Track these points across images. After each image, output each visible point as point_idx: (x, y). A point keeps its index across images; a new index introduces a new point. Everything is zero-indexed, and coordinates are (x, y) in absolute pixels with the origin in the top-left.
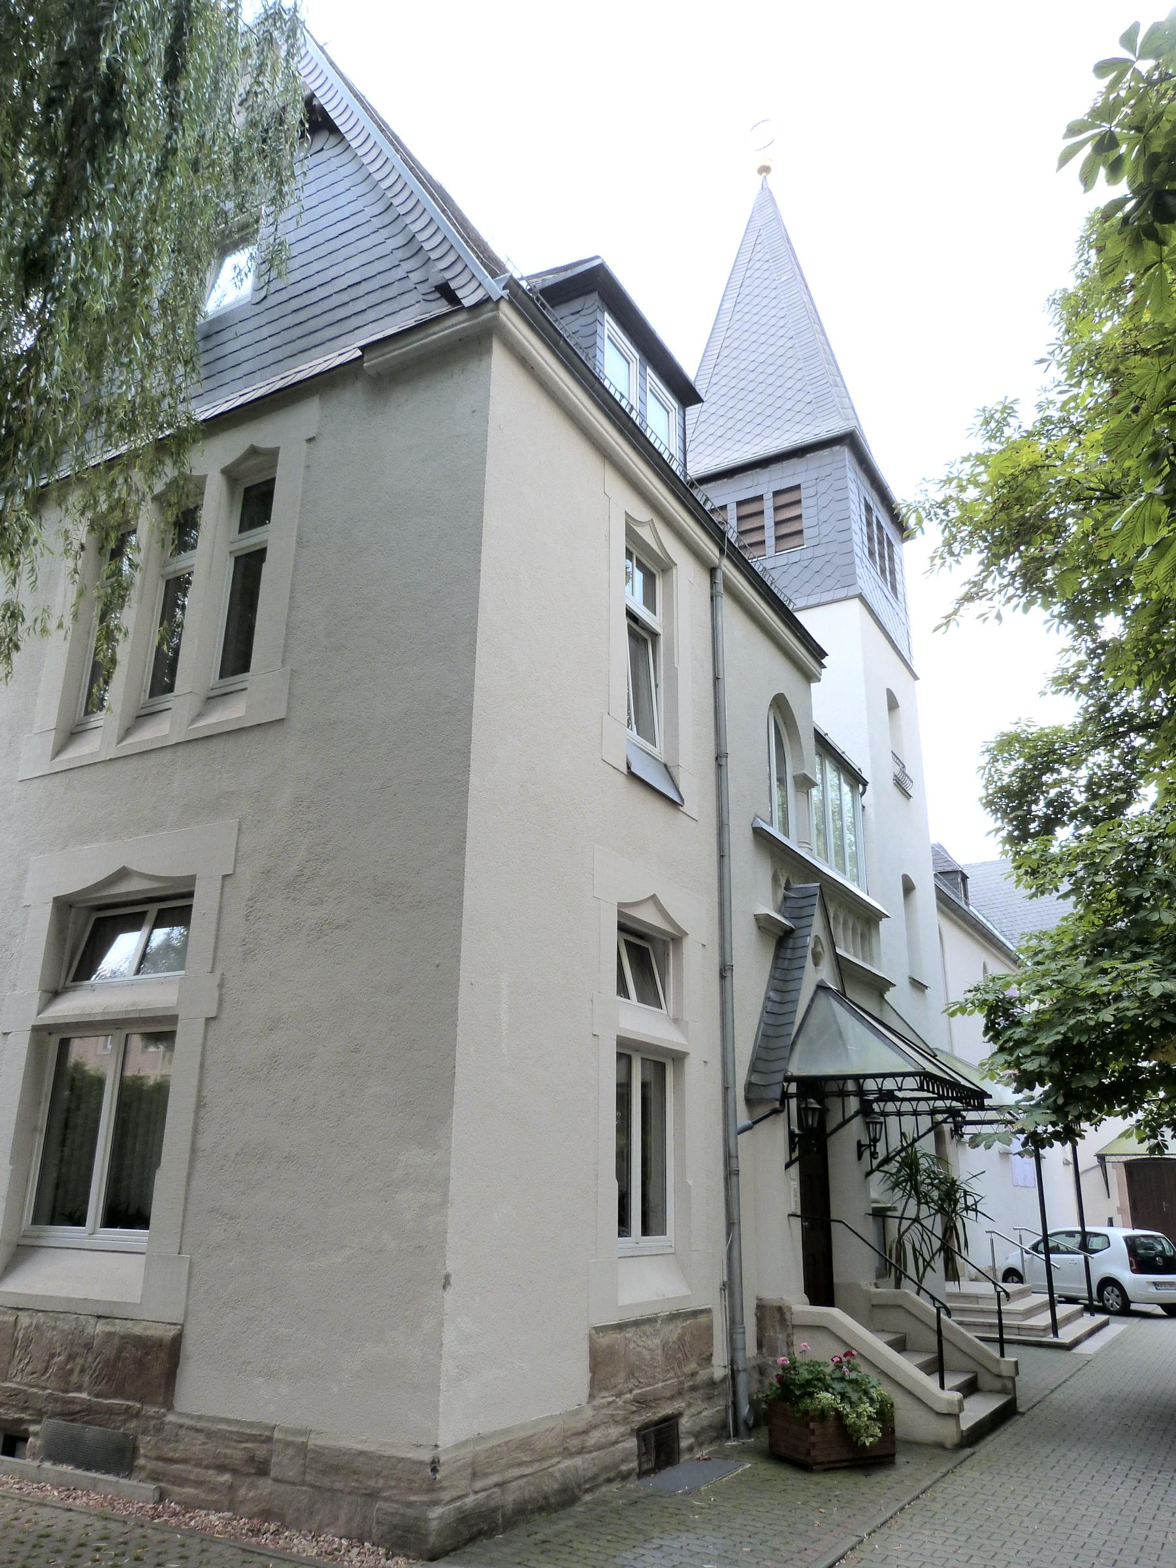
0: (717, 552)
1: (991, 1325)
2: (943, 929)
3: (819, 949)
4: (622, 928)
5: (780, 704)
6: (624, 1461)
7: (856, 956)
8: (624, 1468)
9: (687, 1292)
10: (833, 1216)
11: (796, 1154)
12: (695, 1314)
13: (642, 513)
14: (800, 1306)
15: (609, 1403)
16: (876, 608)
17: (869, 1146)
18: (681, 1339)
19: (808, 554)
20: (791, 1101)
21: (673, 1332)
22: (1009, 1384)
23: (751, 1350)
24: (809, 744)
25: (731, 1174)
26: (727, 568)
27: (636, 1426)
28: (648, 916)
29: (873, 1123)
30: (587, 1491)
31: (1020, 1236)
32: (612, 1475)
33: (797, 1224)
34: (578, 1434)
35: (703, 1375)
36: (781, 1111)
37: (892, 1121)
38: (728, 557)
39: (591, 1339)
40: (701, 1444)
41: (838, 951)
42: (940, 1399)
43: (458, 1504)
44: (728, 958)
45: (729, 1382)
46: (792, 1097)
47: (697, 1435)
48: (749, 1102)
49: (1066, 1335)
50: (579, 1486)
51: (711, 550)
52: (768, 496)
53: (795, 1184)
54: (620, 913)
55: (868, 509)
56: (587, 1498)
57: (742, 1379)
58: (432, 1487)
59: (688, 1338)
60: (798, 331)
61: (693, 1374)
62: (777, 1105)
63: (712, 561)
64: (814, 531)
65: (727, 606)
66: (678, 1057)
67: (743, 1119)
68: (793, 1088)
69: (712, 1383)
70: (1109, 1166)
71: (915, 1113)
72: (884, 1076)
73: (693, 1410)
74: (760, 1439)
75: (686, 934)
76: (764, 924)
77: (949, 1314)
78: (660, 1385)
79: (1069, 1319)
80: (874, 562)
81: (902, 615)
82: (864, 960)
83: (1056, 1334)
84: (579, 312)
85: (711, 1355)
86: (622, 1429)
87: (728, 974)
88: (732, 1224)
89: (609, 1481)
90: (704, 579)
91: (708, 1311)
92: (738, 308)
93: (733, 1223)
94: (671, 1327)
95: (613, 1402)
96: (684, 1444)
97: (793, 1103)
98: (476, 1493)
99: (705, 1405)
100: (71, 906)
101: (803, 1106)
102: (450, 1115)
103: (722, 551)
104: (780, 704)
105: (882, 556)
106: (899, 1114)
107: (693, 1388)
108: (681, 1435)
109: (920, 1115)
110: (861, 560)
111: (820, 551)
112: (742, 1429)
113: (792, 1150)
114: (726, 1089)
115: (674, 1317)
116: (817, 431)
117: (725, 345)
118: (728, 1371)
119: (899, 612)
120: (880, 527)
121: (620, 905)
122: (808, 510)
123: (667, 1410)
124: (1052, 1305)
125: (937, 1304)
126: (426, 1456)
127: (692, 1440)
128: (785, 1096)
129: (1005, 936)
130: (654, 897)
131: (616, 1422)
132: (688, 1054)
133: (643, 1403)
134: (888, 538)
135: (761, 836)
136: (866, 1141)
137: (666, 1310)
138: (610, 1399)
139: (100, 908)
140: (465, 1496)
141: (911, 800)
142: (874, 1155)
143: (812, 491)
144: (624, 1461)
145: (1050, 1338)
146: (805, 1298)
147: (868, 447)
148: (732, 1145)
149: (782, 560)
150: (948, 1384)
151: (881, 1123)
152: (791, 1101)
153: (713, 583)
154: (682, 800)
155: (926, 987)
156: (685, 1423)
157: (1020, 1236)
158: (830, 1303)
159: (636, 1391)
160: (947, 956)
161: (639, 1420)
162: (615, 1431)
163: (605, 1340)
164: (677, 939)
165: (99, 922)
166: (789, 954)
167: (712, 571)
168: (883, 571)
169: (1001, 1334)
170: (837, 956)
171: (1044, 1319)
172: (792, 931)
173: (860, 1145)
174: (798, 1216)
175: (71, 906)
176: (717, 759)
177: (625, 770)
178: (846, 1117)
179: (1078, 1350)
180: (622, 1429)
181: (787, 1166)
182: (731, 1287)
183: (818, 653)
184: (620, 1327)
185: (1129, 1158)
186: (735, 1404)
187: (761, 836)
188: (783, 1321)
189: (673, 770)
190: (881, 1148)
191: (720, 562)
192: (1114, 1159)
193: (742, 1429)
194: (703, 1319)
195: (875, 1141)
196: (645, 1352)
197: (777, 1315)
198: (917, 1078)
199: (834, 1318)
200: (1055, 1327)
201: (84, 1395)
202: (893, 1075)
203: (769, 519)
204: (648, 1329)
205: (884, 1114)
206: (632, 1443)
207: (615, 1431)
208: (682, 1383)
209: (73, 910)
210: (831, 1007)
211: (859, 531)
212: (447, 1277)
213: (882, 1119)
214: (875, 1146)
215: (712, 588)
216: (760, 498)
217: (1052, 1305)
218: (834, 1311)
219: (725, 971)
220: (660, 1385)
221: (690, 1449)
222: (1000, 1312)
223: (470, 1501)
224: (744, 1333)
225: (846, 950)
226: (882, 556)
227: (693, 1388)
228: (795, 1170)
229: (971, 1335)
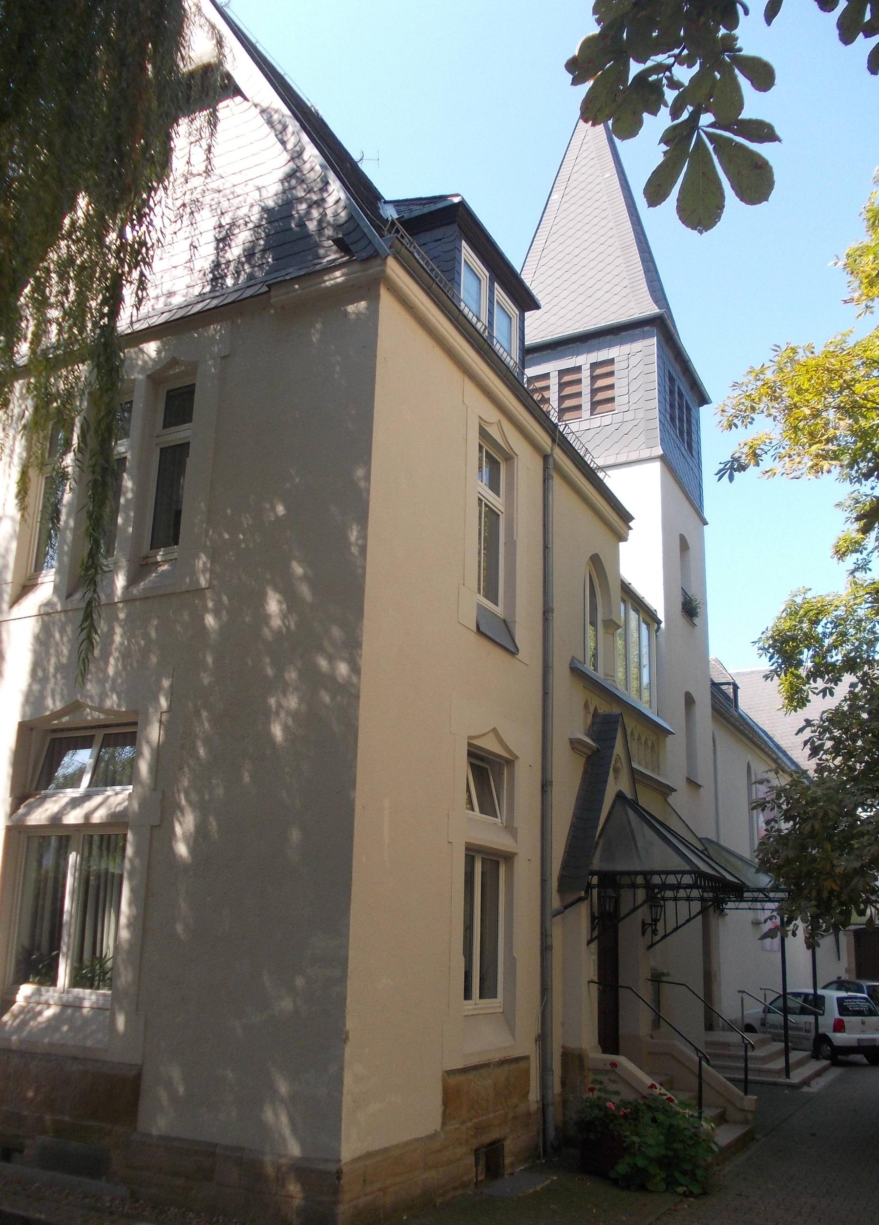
0: (549, 441)
1: (738, 1068)
2: (717, 736)
3: (619, 765)
4: (470, 754)
5: (595, 560)
7: (647, 768)
8: (466, 1179)
10: (620, 984)
11: (595, 934)
12: (517, 1060)
14: (595, 1054)
15: (456, 1129)
17: (651, 925)
19: (619, 418)
20: (593, 890)
23: (557, 1088)
24: (616, 592)
26: (559, 455)
28: (490, 745)
29: (654, 906)
31: (765, 995)
33: (595, 988)
36: (587, 899)
37: (670, 905)
38: (559, 445)
39: (444, 1080)
41: (635, 765)
43: (355, 1203)
46: (594, 888)
48: (561, 890)
49: (796, 1077)
51: (544, 440)
53: (595, 957)
54: (469, 744)
55: (671, 379)
57: (551, 1110)
58: (336, 1191)
60: (618, 223)
61: (516, 1106)
62: (583, 894)
64: (625, 399)
65: (557, 483)
66: (509, 857)
67: (556, 902)
68: (595, 880)
69: (528, 1114)
71: (689, 899)
72: (668, 873)
75: (517, 757)
77: (708, 1062)
78: (492, 1115)
79: (801, 1063)
80: (675, 426)
82: (653, 770)
83: (788, 1076)
85: (528, 1092)
91: (526, 1058)
93: (546, 988)
95: (459, 1128)
97: (595, 892)
98: (365, 1195)
100: (32, 729)
101: (602, 894)
103: (554, 441)
104: (595, 560)
105: (681, 420)
106: (676, 899)
108: (506, 1154)
109: (692, 900)
111: (629, 416)
113: (593, 929)
115: (503, 1062)
116: (631, 312)
117: (555, 223)
120: (681, 395)
121: (470, 738)
123: (494, 1135)
124: (786, 1052)
125: (700, 1055)
126: (333, 1168)
128: (589, 887)
130: (494, 730)
132: (516, 854)
134: (687, 403)
135: (576, 672)
136: (649, 921)
137: (497, 1057)
138: (457, 1126)
139: (55, 731)
140: (359, 1197)
141: (696, 628)
142: (655, 932)
143: (624, 365)
147: (675, 326)
149: (597, 422)
151: (662, 907)
152: (593, 890)
154: (518, 650)
155: (700, 786)
156: (508, 1144)
157: (765, 995)
158: (616, 1052)
159: (475, 1121)
160: (718, 753)
161: (475, 1143)
163: (453, 1081)
164: (510, 763)
165: (53, 741)
167: (546, 458)
168: (681, 433)
169: (746, 1075)
171: (780, 1064)
173: (644, 924)
174: (596, 983)
175: (32, 729)
176: (544, 614)
177: (474, 628)
178: (636, 906)
181: (589, 942)
182: (543, 1039)
183: (626, 518)
184: (464, 1070)
186: (544, 1130)
187: (576, 672)
188: (582, 1066)
189: (510, 625)
190: (660, 926)
191: (552, 449)
194: (522, 1064)
195: (655, 921)
198: (700, 890)
200: (787, 1070)
201: (67, 1118)
202: (674, 873)
204: (483, 1071)
205: (664, 899)
206: (471, 1160)
209: (34, 732)
210: (627, 814)
213: (662, 902)
214: (656, 925)
215: (544, 471)
217: (786, 1052)
218: (621, 1059)
219: (546, 786)
220: (492, 1115)
222: (746, 1059)
223: (362, 1201)
224: (553, 1075)
225: (640, 763)
226: (681, 420)
228: (594, 946)
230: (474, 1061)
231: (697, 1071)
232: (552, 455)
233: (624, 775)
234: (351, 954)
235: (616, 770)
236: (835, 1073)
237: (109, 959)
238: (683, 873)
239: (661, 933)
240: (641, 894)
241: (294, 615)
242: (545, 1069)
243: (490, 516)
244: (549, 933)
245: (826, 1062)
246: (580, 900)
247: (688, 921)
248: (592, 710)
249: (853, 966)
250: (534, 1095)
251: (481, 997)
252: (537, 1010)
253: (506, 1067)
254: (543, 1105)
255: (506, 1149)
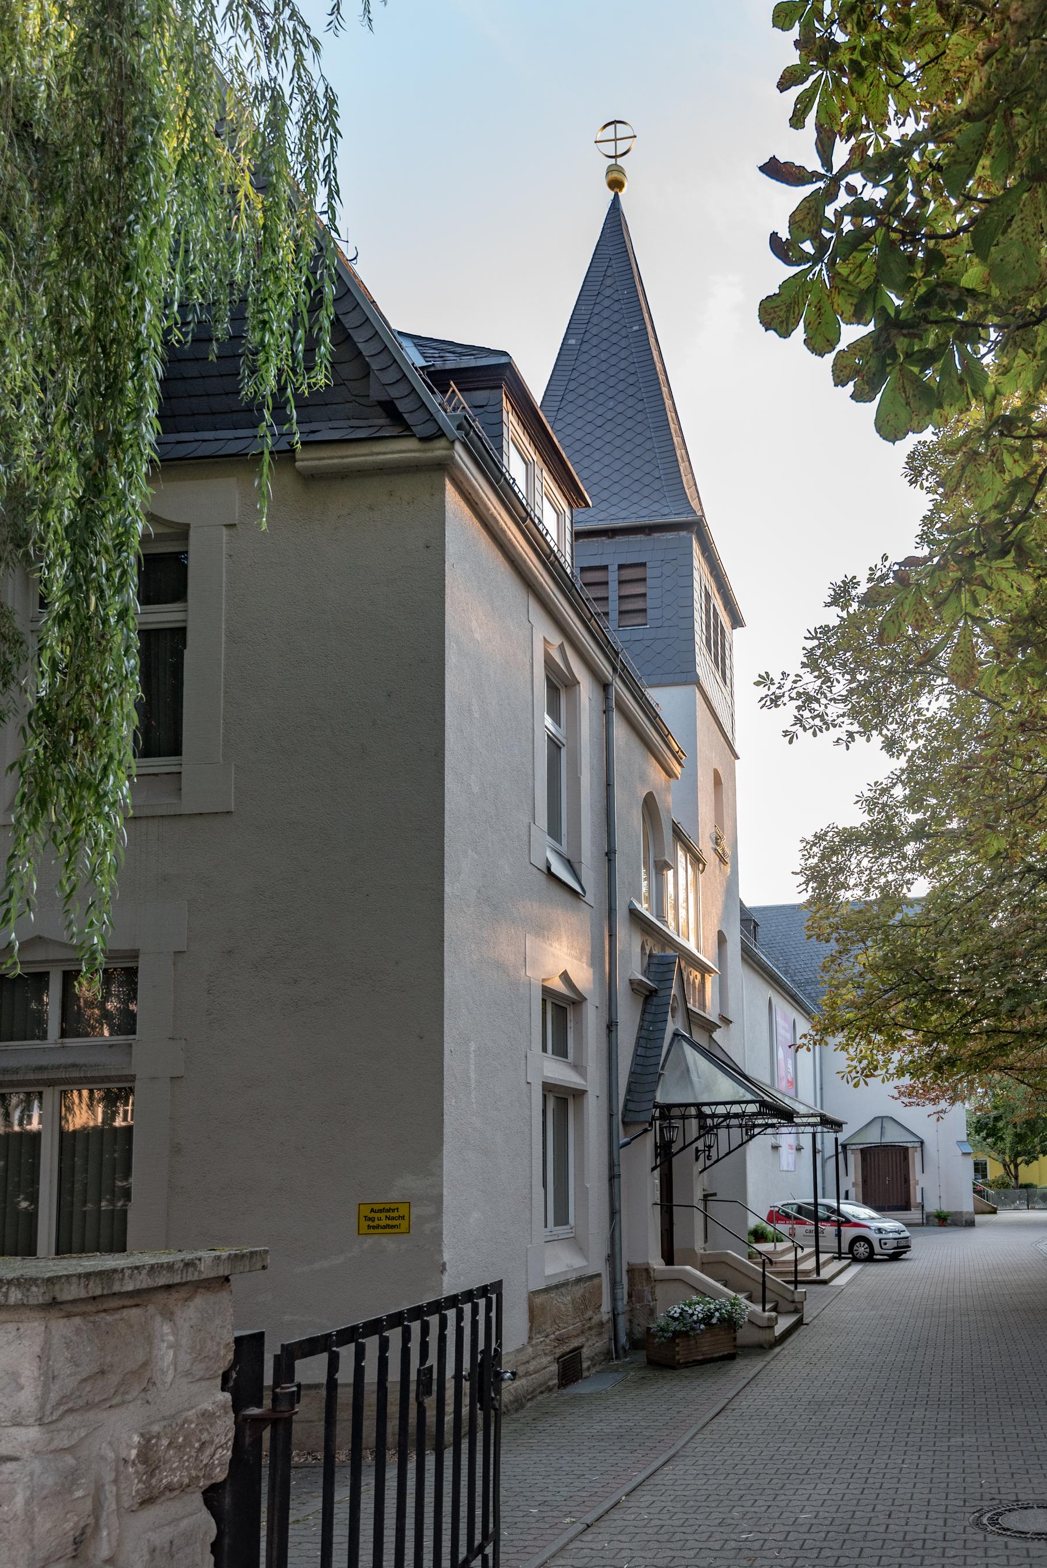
1: (791, 1272)
6: (550, 1379)
8: (551, 1383)
9: (585, 1263)
12: (591, 1278)
13: (556, 639)
16: (715, 704)
17: (704, 1151)
18: (583, 1296)
21: (579, 1290)
22: (799, 1306)
25: (613, 1177)
26: (618, 686)
27: (557, 1356)
30: (529, 1400)
32: (543, 1388)
34: (524, 1364)
35: (596, 1319)
40: (594, 1365)
41: (690, 1006)
42: (762, 1318)
44: (614, 1016)
45: (611, 1324)
47: (592, 1359)
49: (825, 1273)
50: (525, 1397)
52: (613, 568)
56: (529, 1405)
59: (587, 1295)
63: (607, 678)
66: (579, 1094)
69: (601, 1324)
70: (849, 1153)
73: (590, 1343)
74: (641, 1356)
75: (586, 999)
76: (635, 986)
81: (729, 699)
83: (818, 1274)
84: (482, 407)
86: (549, 1358)
87: (613, 1029)
88: (614, 1213)
89: (542, 1392)
90: (599, 694)
91: (599, 1275)
92: (585, 348)
94: (578, 1287)
96: (585, 1365)
99: (597, 1339)
102: (441, 1151)
103: (615, 669)
106: (728, 1127)
107: (590, 1328)
110: (700, 649)
112: (621, 1352)
114: (611, 1115)
115: (579, 1280)
118: (611, 1315)
119: (726, 695)
122: (652, 589)
123: (575, 1343)
124: (817, 1253)
127: (589, 1363)
129: (777, 968)
131: (545, 1354)
132: (586, 1091)
133: (560, 1340)
137: (573, 1276)
142: (709, 1157)
144: (550, 1379)
145: (814, 1277)
146: (662, 1261)
148: (615, 1156)
150: (767, 1308)
153: (607, 698)
156: (586, 1352)
159: (557, 1333)
161: (559, 1352)
162: (545, 1360)
163: (538, 1300)
166: (653, 1009)
167: (605, 687)
169: (796, 1277)
170: (688, 1009)
172: (656, 991)
179: (834, 1283)
180: (549, 1358)
181: (653, 1169)
182: (612, 1259)
184: (547, 1290)
185: (861, 1146)
188: (649, 1277)
189: (576, 866)
192: (854, 1147)
193: (621, 1352)
194: (596, 1281)
196: (562, 1306)
197: (644, 1274)
199: (687, 1273)
203: (613, 591)
204: (563, 1290)
206: (554, 1368)
207: (545, 1360)
208: (583, 1325)
211: (699, 620)
212: (444, 1265)
216: (605, 568)
217: (817, 1253)
219: (611, 1026)
221: (589, 1368)
225: (694, 1006)
227: (590, 1328)
229: (779, 1280)
230: (554, 1282)
231: (761, 1280)
232: (612, 684)
233: (680, 1014)
234: (445, 1192)
235: (674, 1010)
236: (855, 1269)
237: (17, 1106)
238: (747, 1102)
239: (714, 1158)
240: (694, 1123)
241: (899, 144)
242: (614, 1284)
243: (554, 745)
244: (616, 1163)
245: (848, 1261)
246: (646, 1131)
247: (740, 1146)
248: (648, 952)
249: (860, 1179)
250: (606, 1307)
251: (555, 1225)
252: (606, 1234)
253: (583, 1285)
254: (614, 1315)
255: (584, 1356)
